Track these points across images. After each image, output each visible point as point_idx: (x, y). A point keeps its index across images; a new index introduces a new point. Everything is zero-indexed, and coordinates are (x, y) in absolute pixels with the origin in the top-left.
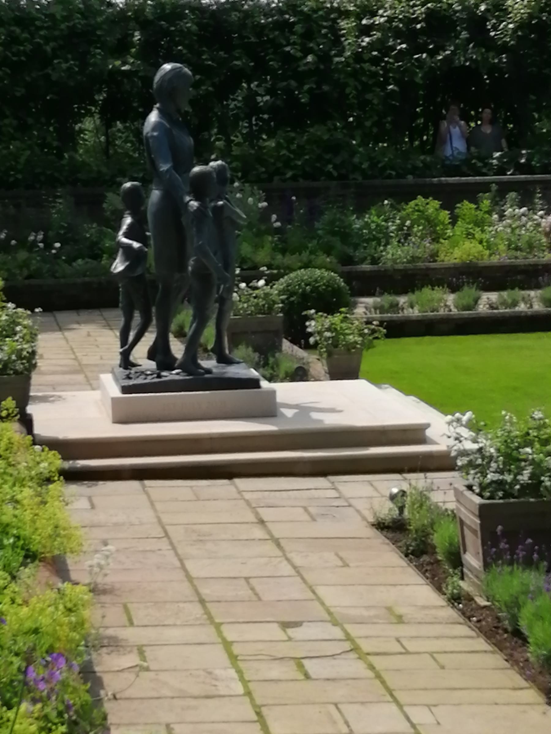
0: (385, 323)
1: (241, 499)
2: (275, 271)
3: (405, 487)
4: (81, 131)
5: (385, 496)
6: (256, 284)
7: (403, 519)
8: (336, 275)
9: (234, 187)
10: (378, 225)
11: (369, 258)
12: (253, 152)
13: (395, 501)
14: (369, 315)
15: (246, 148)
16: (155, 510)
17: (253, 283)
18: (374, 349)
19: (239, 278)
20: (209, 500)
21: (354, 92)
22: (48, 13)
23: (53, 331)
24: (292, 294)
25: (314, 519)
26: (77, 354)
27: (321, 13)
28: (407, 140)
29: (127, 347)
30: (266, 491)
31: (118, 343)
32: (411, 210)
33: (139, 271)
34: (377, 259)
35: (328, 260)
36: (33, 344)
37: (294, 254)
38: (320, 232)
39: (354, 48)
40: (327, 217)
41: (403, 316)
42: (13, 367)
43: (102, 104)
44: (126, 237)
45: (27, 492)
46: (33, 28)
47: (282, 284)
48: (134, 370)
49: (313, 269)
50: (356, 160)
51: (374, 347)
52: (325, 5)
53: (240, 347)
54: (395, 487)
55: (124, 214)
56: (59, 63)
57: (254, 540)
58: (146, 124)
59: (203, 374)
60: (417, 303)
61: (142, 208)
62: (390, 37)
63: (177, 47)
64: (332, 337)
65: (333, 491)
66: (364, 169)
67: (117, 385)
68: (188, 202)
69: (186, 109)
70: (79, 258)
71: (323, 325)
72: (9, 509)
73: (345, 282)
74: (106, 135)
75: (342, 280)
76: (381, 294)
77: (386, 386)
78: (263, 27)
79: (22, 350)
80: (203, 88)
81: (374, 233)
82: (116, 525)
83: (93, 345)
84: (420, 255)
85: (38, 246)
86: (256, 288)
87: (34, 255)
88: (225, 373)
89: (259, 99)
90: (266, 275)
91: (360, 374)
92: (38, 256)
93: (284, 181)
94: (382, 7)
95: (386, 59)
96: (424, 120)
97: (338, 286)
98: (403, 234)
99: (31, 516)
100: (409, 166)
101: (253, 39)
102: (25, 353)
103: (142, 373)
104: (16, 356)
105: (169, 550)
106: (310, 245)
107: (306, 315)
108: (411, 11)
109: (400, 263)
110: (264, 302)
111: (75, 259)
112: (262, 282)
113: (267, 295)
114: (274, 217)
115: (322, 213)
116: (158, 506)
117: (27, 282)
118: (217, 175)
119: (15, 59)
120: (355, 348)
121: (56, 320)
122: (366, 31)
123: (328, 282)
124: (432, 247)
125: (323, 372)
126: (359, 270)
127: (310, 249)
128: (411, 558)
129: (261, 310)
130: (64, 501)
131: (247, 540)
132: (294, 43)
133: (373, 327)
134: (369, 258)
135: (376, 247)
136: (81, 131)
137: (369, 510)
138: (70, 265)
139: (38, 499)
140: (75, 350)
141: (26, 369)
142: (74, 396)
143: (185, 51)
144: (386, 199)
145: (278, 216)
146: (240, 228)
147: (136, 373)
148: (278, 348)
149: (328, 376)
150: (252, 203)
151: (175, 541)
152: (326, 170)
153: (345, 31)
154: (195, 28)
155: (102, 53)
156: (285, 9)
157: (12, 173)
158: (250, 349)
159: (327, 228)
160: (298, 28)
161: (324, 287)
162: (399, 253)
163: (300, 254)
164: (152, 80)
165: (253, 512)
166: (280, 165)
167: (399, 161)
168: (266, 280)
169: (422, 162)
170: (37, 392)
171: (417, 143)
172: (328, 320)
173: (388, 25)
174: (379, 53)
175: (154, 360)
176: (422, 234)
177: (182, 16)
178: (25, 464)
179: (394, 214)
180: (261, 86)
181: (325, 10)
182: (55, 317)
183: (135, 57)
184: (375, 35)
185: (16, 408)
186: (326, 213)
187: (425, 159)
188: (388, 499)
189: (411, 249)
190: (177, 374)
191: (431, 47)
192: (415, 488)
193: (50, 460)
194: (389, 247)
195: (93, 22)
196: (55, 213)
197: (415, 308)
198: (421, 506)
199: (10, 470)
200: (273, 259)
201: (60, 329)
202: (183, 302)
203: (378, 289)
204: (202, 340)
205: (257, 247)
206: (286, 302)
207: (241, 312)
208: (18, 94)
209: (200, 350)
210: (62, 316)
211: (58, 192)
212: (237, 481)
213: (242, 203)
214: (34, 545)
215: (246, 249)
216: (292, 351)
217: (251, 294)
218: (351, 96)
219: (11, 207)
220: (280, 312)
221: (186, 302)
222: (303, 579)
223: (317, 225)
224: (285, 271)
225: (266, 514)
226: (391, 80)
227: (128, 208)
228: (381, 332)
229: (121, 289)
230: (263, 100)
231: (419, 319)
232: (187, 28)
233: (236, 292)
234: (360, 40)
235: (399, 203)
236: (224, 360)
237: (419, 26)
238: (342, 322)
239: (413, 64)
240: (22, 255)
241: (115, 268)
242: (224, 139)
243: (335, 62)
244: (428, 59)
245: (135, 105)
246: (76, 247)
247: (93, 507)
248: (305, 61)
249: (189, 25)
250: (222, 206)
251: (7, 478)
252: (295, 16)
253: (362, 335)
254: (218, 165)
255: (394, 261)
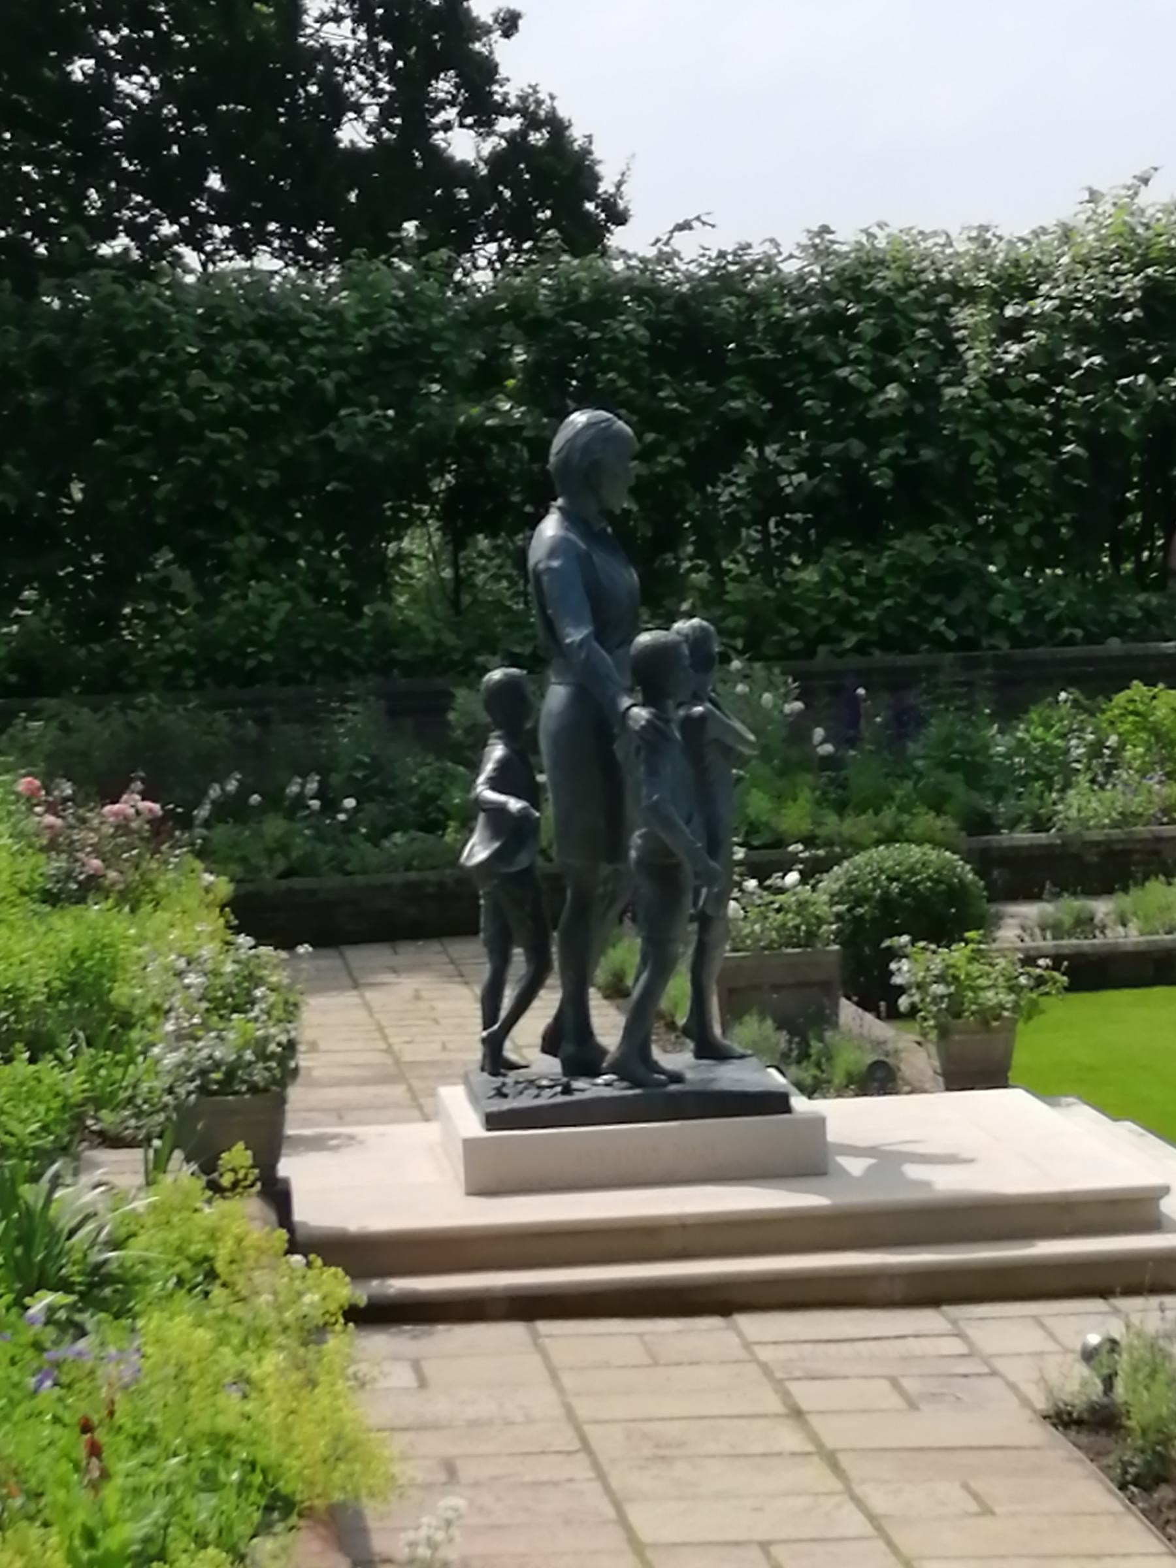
0: (1066, 963)
2: (821, 852)
3: (1116, 1329)
5: (1072, 1351)
6: (779, 882)
7: (1114, 1404)
8: (956, 857)
9: (728, 671)
10: (1046, 747)
11: (1027, 817)
12: (770, 593)
14: (1029, 943)
15: (756, 587)
16: (561, 1390)
17: (774, 880)
20: (679, 1364)
23: (340, 988)
24: (859, 900)
26: (392, 1040)
27: (913, 293)
28: (1106, 560)
29: (496, 1027)
31: (478, 1021)
32: (1117, 712)
33: (522, 861)
34: (1045, 818)
35: (939, 823)
36: (289, 1026)
37: (864, 812)
38: (919, 763)
39: (985, 367)
40: (935, 730)
41: (1103, 945)
43: (444, 499)
44: (493, 788)
45: (273, 1360)
46: (294, 342)
48: (512, 1076)
49: (905, 845)
50: (997, 605)
51: (1042, 1012)
53: (747, 1018)
56: (353, 415)
57: (779, 1454)
58: (534, 542)
59: (664, 1084)
60: (1135, 914)
61: (529, 725)
64: (950, 995)
66: (1014, 626)
69: (625, 505)
70: (395, 830)
71: (928, 969)
72: (231, 1400)
73: (976, 872)
74: (456, 566)
75: (968, 867)
76: (1057, 896)
77: (1071, 1100)
78: (791, 327)
79: (266, 1039)
80: (662, 459)
81: (1038, 763)
82: (473, 1424)
83: (424, 1018)
84: (1141, 810)
85: (308, 807)
86: (781, 891)
87: (299, 825)
88: (713, 1080)
89: (784, 481)
90: (801, 861)
92: (308, 828)
93: (842, 654)
94: (1048, 277)
95: (1058, 390)
96: (1144, 517)
97: (961, 881)
98: (1101, 765)
100: (1113, 617)
101: (768, 354)
102: (272, 1047)
103: (531, 1082)
104: (254, 1052)
105: (589, 1480)
106: (899, 793)
107: (889, 948)
108: (1112, 285)
109: (1096, 826)
110: (798, 920)
111: (387, 833)
112: (793, 877)
113: (802, 905)
114: (819, 733)
115: (922, 722)
116: (567, 1380)
117: (284, 884)
118: (692, 650)
119: (257, 408)
120: (998, 1017)
121: (347, 966)
122: (1013, 330)
124: (1166, 791)
125: (931, 1073)
127: (898, 801)
129: (792, 937)
132: (858, 361)
133: (1038, 971)
134: (1027, 817)
135: (1042, 792)
136: (402, 557)
137: (1037, 1383)
138: (376, 845)
139: (296, 1377)
140: (387, 1031)
141: (275, 1081)
142: (383, 1135)
143: (621, 383)
144: (1063, 690)
145: (826, 729)
146: (743, 762)
147: (517, 1083)
148: (826, 1019)
149: (940, 1079)
150: (770, 705)
151: (603, 1460)
152: (931, 629)
153: (964, 332)
154: (642, 332)
156: (835, 288)
157: (250, 650)
158: (769, 1022)
159: (934, 754)
160: (867, 327)
161: (929, 884)
162: (1094, 804)
163: (876, 813)
164: (549, 443)
165: (776, 1392)
166: (829, 620)
167: (1089, 606)
168: (801, 872)
169: (1141, 607)
170: (302, 1127)
171: (1128, 566)
172: (939, 958)
173: (1061, 316)
175: (555, 1056)
176: (1144, 763)
177: (616, 309)
180: (788, 453)
181: (924, 287)
182: (342, 956)
184: (1033, 337)
185: (253, 1167)
186: (933, 721)
187: (1147, 602)
188: (1078, 1356)
189: (1120, 797)
190: (608, 1085)
191: (1155, 360)
192: (1139, 1335)
193: (325, 1288)
194: (1071, 792)
195: (423, 326)
196: (344, 735)
197: (1130, 925)
198: (1153, 1375)
200: (818, 823)
201: (356, 985)
202: (621, 921)
203: (1048, 885)
204: (664, 1004)
205: (780, 798)
206: (848, 917)
207: (749, 942)
208: (264, 484)
209: (658, 1027)
210: (360, 956)
212: (743, 1321)
213: (749, 703)
214: (287, 1482)
215: (758, 803)
217: (772, 903)
218: (981, 471)
219: (249, 723)
220: (834, 941)
221: (627, 922)
222: (890, 1543)
223: (912, 747)
224: (843, 850)
225: (806, 1394)
226: (1069, 435)
228: (1055, 983)
231: (1142, 948)
232: (626, 333)
233: (735, 899)
234: (999, 350)
236: (709, 1050)
237: (1128, 316)
238: (971, 960)
239: (1117, 399)
240: (275, 826)
241: (470, 856)
242: (708, 567)
244: (1150, 386)
245: (516, 498)
246: (390, 807)
247: (423, 1383)
248: (881, 398)
249: (629, 327)
250: (702, 717)
251: (232, 1328)
252: (858, 302)
254: (693, 628)
255: (1084, 823)
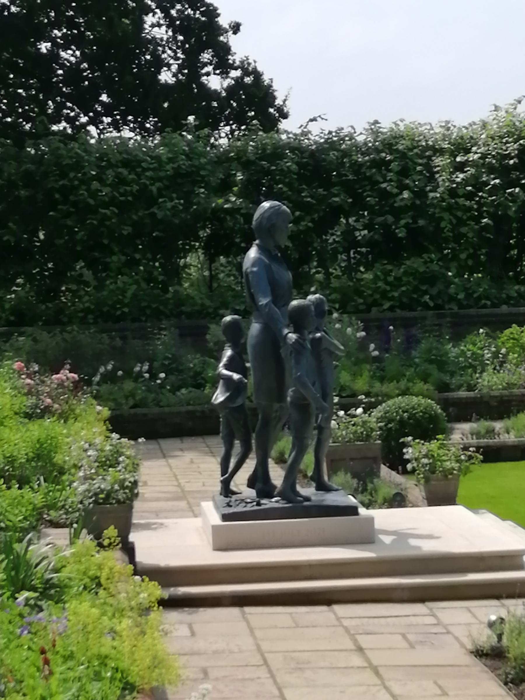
1: (339, 626)
2: (373, 400)
3: (503, 614)
4: (187, 266)
5: (484, 623)
7: (502, 647)
8: (433, 402)
11: (465, 385)
12: (351, 284)
13: (493, 628)
14: (466, 441)
17: (352, 411)
18: (471, 474)
19: (337, 407)
20: (307, 627)
21: (448, 225)
22: (154, 155)
23: (158, 458)
24: (390, 421)
25: (412, 646)
26: (180, 481)
27: (416, 151)
30: (364, 617)
31: (219, 473)
32: (505, 338)
33: (239, 402)
36: (135, 474)
37: (392, 381)
38: (417, 360)
40: (424, 345)
42: (115, 497)
45: (126, 623)
46: (139, 170)
47: (380, 412)
48: (234, 497)
49: (410, 396)
50: (452, 290)
52: (420, 143)
53: (339, 473)
54: (493, 614)
55: (224, 347)
56: (165, 202)
57: (352, 667)
59: (302, 502)
60: (513, 428)
61: (243, 341)
62: (484, 172)
63: (278, 185)
64: (430, 464)
65: (432, 617)
66: (460, 299)
67: (218, 513)
68: (287, 334)
71: (420, 452)
72: (107, 640)
73: (442, 409)
74: (210, 270)
75: (438, 407)
77: (484, 511)
79: (124, 480)
80: (303, 223)
81: (470, 360)
82: (216, 652)
83: (195, 472)
84: (516, 382)
85: (143, 377)
86: (355, 416)
88: (323, 500)
89: (357, 234)
90: (364, 403)
91: (457, 499)
95: (480, 194)
96: (518, 252)
97: (435, 412)
99: (130, 647)
100: (504, 296)
101: (351, 177)
102: (127, 483)
104: (119, 486)
105: (267, 678)
106: (408, 373)
107: (403, 442)
109: (496, 389)
110: (362, 430)
111: (179, 388)
112: (360, 410)
113: (364, 423)
114: (372, 346)
115: (418, 342)
116: (258, 633)
117: (133, 411)
119: (122, 198)
120: (452, 474)
122: (460, 167)
123: (425, 409)
125: (421, 498)
126: (455, 397)
127: (407, 377)
128: (511, 687)
129: (359, 437)
130: (163, 630)
131: (345, 668)
132: (391, 180)
133: (470, 453)
134: (465, 385)
135: (472, 374)
136: (187, 266)
137: (468, 637)
138: (174, 394)
139: (137, 630)
140: (178, 477)
141: (128, 499)
142: (176, 523)
143: (285, 189)
144: (482, 328)
145: (375, 345)
146: (338, 358)
147: (236, 500)
148: (375, 474)
149: (426, 501)
151: (273, 669)
152: (423, 301)
153: (439, 168)
154: (294, 167)
155: (206, 192)
156: (381, 148)
157: (118, 306)
158: (349, 474)
161: (421, 414)
162: (495, 379)
163: (398, 382)
164: (253, 215)
165: (351, 640)
166: (377, 296)
167: (493, 291)
168: (363, 408)
169: (517, 292)
173: (482, 161)
174: (473, 188)
175: (253, 488)
177: (282, 156)
178: (125, 595)
179: (489, 343)
182: (159, 444)
183: (238, 196)
184: (469, 171)
185: (118, 537)
187: (519, 289)
188: (486, 625)
192: (513, 616)
194: (485, 374)
195: (196, 163)
196: (160, 345)
197: (511, 433)
199: (110, 600)
200: (371, 387)
201: (164, 456)
202: (283, 429)
204: (302, 466)
205: (355, 375)
206: (384, 428)
207: (340, 439)
208: (125, 233)
209: (300, 476)
210: (166, 443)
211: (162, 324)
213: (341, 333)
215: (345, 377)
216: (390, 477)
218: (445, 231)
219: (118, 339)
221: (286, 430)
223: (414, 353)
224: (383, 398)
225: (364, 641)
226: (485, 214)
227: (228, 341)
229: (221, 419)
230: (362, 234)
231: (516, 444)
235: (494, 331)
236: (322, 487)
237: (511, 162)
238: (439, 448)
239: (506, 198)
240: (129, 385)
241: (216, 399)
243: (430, 198)
244: (521, 194)
245: (237, 240)
246: (180, 377)
248: (401, 197)
250: (320, 339)
251: (108, 608)
253: (459, 461)
254: (316, 298)
255: (490, 388)
